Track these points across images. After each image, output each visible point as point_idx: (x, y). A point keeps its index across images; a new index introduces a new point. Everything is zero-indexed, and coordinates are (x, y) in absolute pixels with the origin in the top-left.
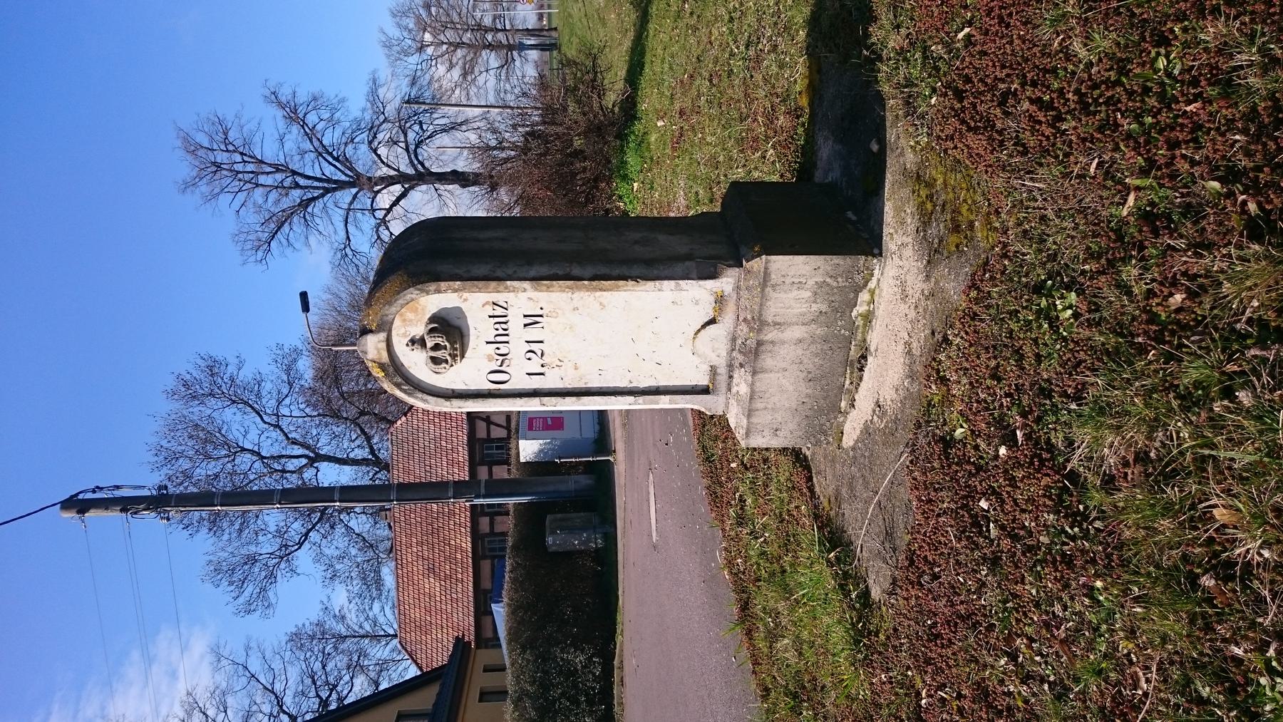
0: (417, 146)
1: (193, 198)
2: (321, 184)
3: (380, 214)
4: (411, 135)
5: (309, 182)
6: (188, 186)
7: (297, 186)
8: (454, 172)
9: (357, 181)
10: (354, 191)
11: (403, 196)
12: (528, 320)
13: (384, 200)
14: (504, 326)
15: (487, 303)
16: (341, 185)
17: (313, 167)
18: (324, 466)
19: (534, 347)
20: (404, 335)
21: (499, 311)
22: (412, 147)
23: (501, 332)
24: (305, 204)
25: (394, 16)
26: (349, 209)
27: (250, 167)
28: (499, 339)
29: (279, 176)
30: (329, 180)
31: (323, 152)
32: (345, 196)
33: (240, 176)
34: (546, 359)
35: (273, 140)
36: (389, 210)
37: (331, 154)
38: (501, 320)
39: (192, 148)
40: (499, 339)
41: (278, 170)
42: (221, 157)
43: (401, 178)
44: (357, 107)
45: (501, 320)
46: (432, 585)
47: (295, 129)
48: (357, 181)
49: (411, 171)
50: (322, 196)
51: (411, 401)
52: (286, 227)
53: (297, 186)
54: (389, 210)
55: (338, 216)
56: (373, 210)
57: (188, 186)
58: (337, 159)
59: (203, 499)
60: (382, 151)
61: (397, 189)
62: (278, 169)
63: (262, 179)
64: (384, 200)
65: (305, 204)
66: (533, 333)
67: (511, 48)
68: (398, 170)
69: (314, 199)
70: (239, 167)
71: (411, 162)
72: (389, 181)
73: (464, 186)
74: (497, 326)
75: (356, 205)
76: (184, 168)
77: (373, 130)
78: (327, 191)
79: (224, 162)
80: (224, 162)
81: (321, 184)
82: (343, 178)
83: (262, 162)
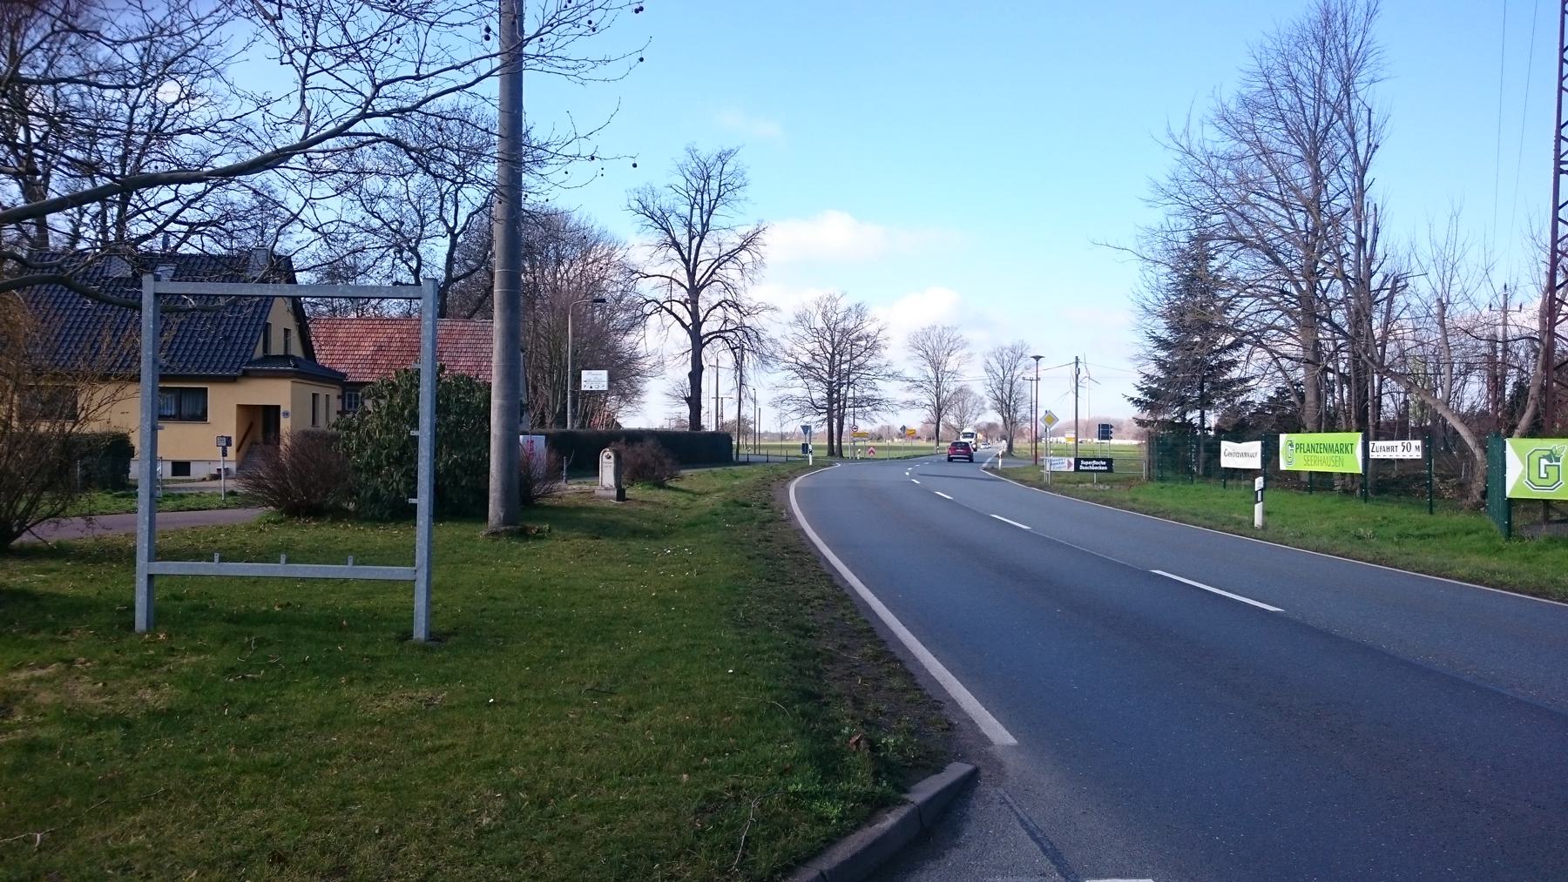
1: (683, 157)
4: (732, 335)
6: (692, 152)
7: (691, 239)
8: (702, 368)
9: (695, 290)
10: (687, 284)
11: (683, 324)
13: (678, 309)
16: (691, 275)
18: (447, 241)
24: (676, 245)
25: (858, 306)
27: (706, 207)
29: (699, 228)
30: (695, 266)
31: (719, 262)
32: (683, 276)
35: (728, 227)
36: (670, 312)
39: (722, 158)
43: (697, 324)
44: (751, 295)
46: (367, 348)
47: (739, 241)
48: (695, 290)
49: (704, 331)
50: (683, 259)
51: (497, 313)
53: (691, 239)
55: (667, 269)
57: (692, 152)
59: (635, 533)
60: (719, 310)
61: (688, 320)
62: (705, 225)
63: (697, 212)
64: (678, 309)
65: (676, 245)
67: (830, 411)
72: (694, 314)
73: (690, 375)
75: (675, 285)
76: (708, 150)
77: (736, 306)
78: (687, 262)
79: (709, 186)
80: (709, 186)
82: (697, 278)
83: (710, 213)
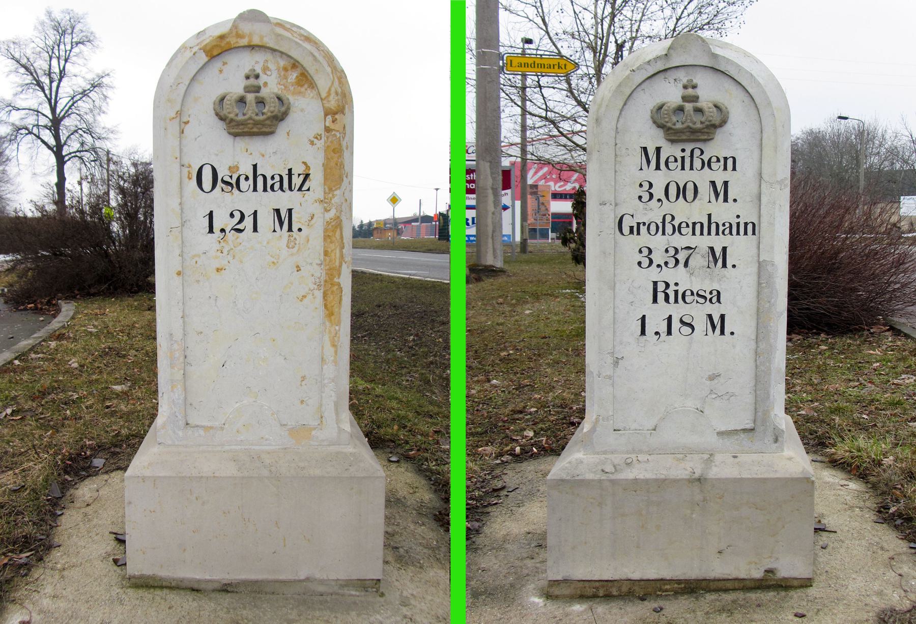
0: (81, 158)
2: (53, 97)
3: (35, 131)
4: (87, 155)
5: (54, 89)
6: (49, 13)
7: (51, 82)
11: (49, 147)
12: (284, 214)
14: (277, 186)
15: (308, 167)
16: (53, 110)
17: (67, 89)
19: (248, 222)
20: (265, 69)
21: (297, 181)
22: (78, 154)
23: (270, 182)
26: (38, 112)
28: (260, 181)
31: (73, 101)
33: (56, 47)
34: (231, 235)
36: (38, 137)
37: (73, 105)
38: (285, 182)
40: (260, 181)
41: (61, 72)
42: (68, 39)
45: (285, 182)
49: (64, 153)
50: (46, 96)
52: (22, 70)
54: (38, 137)
56: (38, 126)
57: (49, 13)
58: (70, 108)
61: (52, 142)
63: (54, 62)
65: (39, 84)
66: (266, 220)
68: (65, 144)
69: (43, 90)
70: (62, 47)
71: (70, 153)
74: (277, 178)
77: (89, 131)
78: (50, 100)
81: (53, 97)
82: (58, 111)
